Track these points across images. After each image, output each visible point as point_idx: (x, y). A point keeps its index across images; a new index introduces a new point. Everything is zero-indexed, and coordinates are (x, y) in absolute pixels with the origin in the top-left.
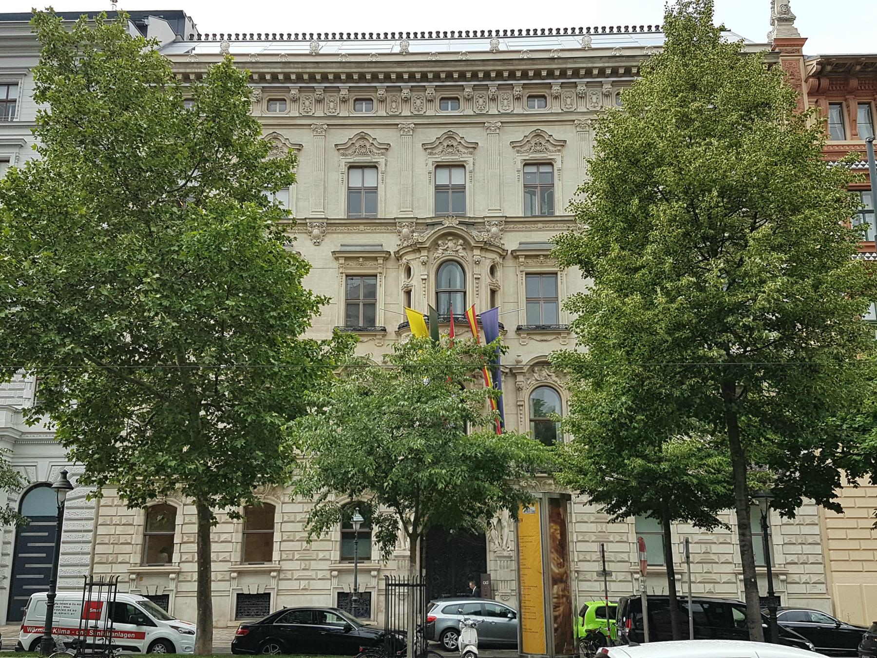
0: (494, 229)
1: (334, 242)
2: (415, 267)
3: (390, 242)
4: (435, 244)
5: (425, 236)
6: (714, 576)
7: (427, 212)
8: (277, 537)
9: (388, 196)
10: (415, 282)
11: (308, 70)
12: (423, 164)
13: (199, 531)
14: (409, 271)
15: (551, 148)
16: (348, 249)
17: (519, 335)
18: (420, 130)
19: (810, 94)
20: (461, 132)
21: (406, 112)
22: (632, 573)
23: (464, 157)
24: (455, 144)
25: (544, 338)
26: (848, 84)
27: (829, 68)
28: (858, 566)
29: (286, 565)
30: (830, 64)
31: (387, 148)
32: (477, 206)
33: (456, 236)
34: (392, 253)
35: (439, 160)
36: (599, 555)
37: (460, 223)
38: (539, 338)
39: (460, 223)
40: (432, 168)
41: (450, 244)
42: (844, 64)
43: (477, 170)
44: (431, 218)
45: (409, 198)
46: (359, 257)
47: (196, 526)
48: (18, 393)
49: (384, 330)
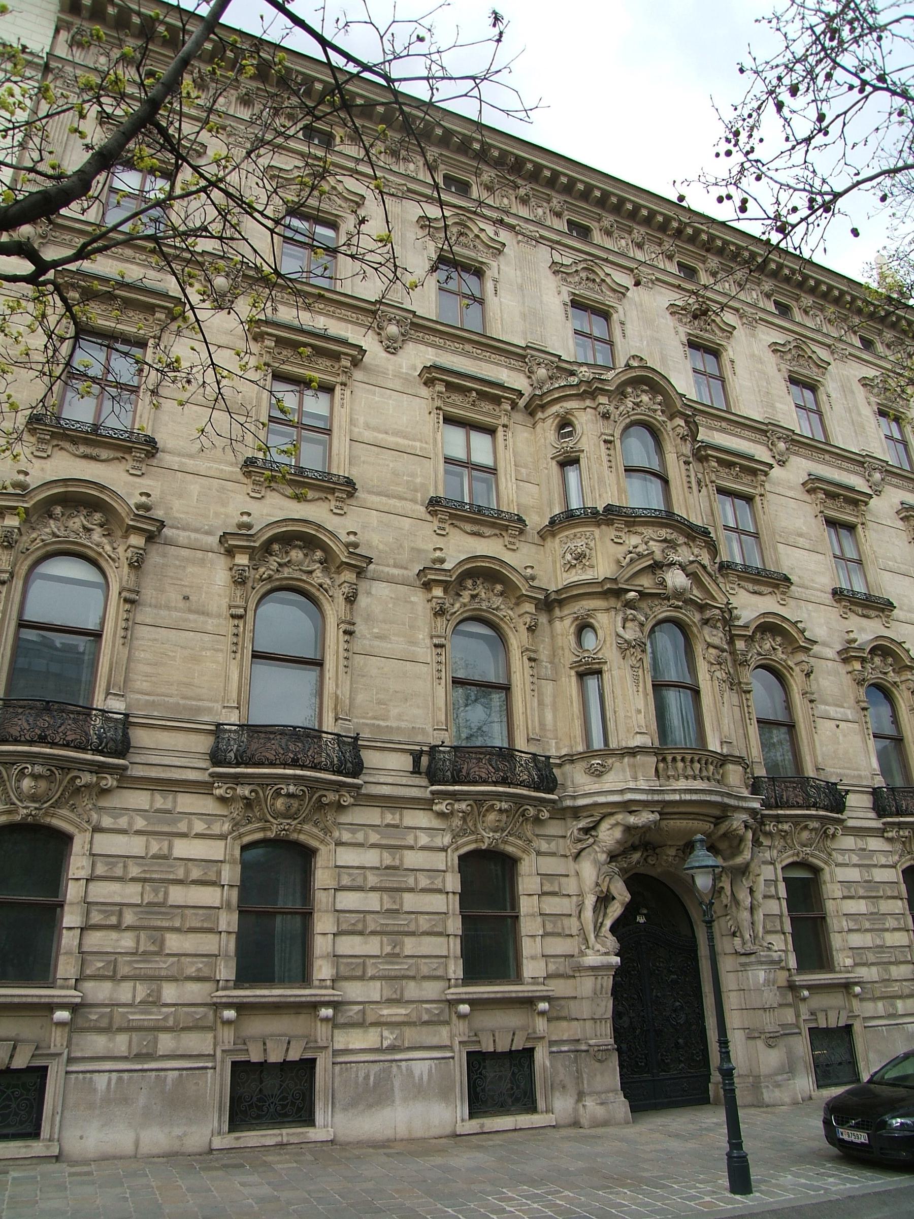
46: (471, 390)
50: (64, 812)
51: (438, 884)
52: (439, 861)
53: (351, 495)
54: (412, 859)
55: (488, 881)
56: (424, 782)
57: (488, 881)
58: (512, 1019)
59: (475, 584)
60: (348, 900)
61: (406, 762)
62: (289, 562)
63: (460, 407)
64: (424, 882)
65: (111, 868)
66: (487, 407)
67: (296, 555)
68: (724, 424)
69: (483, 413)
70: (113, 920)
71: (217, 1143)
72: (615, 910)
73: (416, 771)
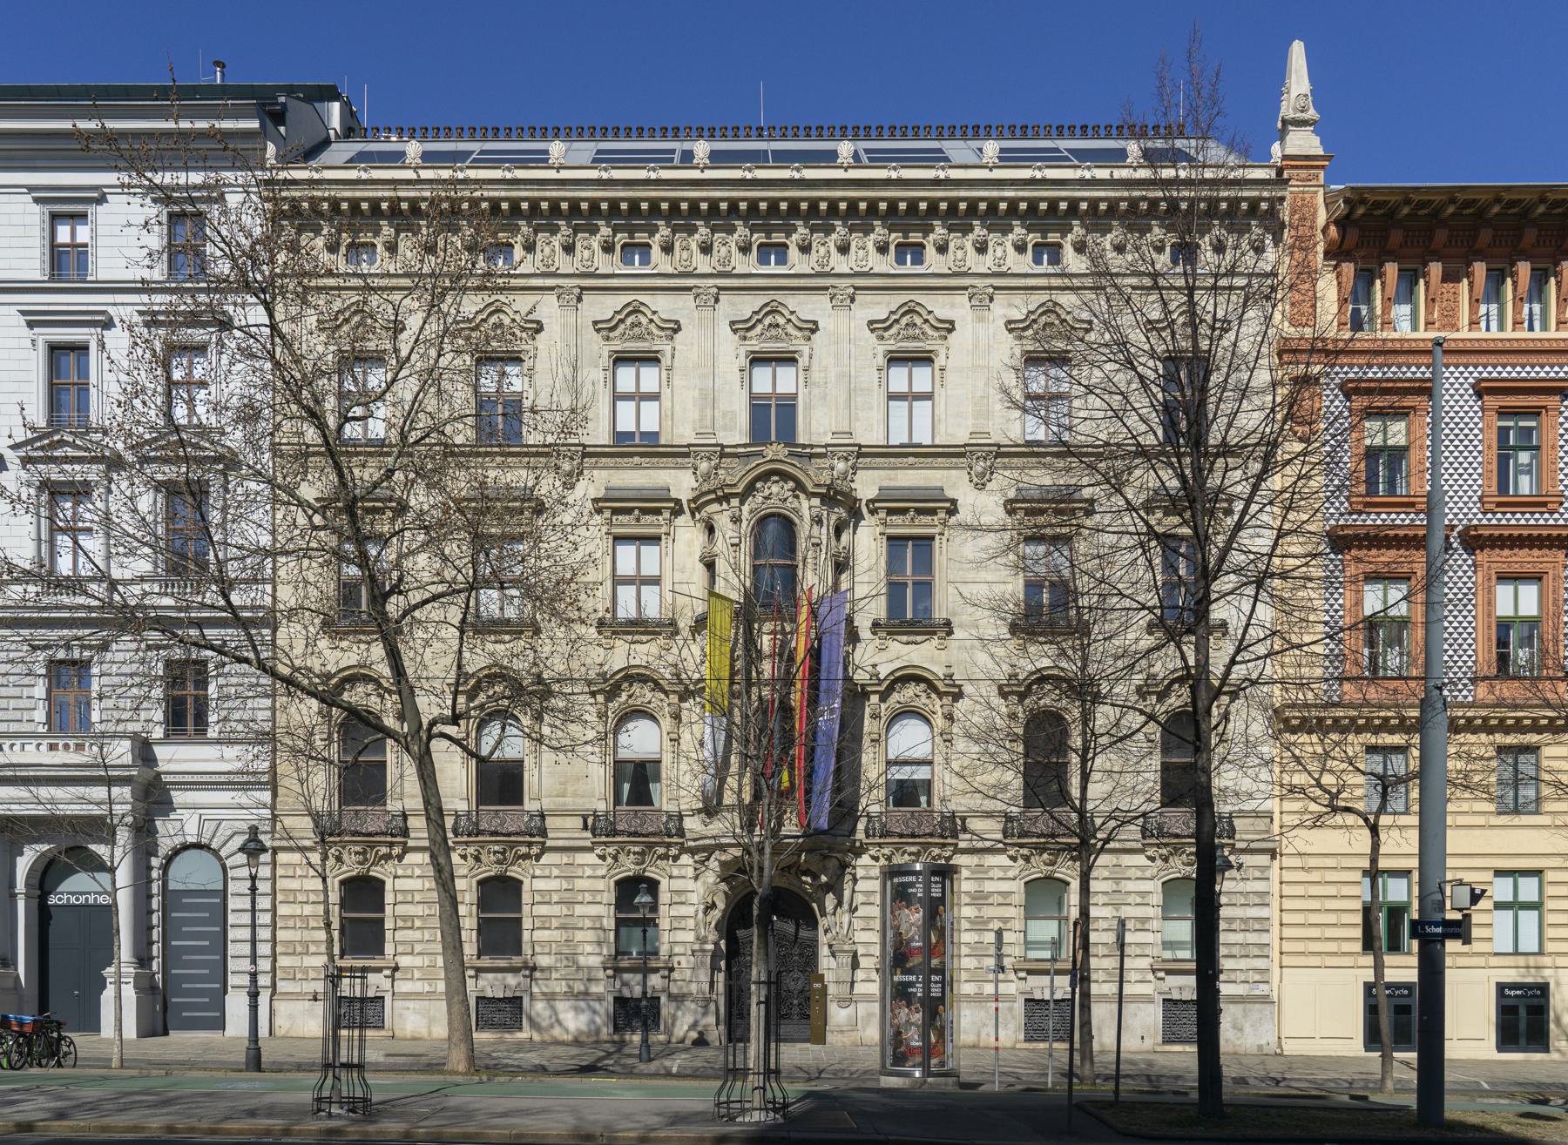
0: (841, 466)
1: (1004, 483)
2: (723, 521)
3: (682, 484)
4: (750, 489)
5: (735, 474)
6: (574, 920)
7: (736, 433)
8: (527, 924)
9: (677, 408)
10: (720, 546)
11: (548, 194)
12: (731, 353)
13: (1442, 973)
14: (711, 530)
15: (930, 332)
16: (617, 494)
17: (874, 633)
18: (999, 298)
19: (1328, 255)
20: (791, 301)
21: (704, 268)
22: (1154, 971)
23: (797, 343)
24: (781, 321)
25: (912, 638)
26: (1431, 238)
27: (1361, 211)
28: (1315, 961)
29: (404, 961)
30: (1363, 201)
31: (814, 328)
32: (815, 426)
33: (785, 476)
34: (685, 503)
35: (619, 348)
36: (1127, 950)
37: (791, 454)
38: (904, 638)
39: (791, 454)
40: (743, 361)
41: (775, 489)
42: (1386, 202)
43: (815, 368)
44: (745, 446)
45: (709, 412)
46: (633, 509)
47: (1416, 971)
48: (26, 692)
49: (948, 624)
50: (515, 868)
51: (598, 899)
52: (600, 884)
53: (950, 633)
54: (580, 884)
55: (634, 895)
56: (589, 835)
57: (634, 895)
58: (512, 980)
59: (631, 685)
60: (542, 910)
61: (579, 822)
62: (611, 694)
63: (626, 524)
64: (588, 897)
65: (545, 898)
66: (649, 518)
67: (636, 688)
68: (911, 460)
69: (648, 525)
70: (409, 924)
71: (1159, 1049)
72: (716, 914)
73: (585, 827)
